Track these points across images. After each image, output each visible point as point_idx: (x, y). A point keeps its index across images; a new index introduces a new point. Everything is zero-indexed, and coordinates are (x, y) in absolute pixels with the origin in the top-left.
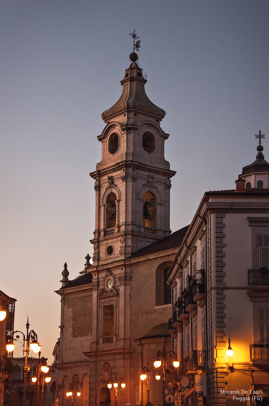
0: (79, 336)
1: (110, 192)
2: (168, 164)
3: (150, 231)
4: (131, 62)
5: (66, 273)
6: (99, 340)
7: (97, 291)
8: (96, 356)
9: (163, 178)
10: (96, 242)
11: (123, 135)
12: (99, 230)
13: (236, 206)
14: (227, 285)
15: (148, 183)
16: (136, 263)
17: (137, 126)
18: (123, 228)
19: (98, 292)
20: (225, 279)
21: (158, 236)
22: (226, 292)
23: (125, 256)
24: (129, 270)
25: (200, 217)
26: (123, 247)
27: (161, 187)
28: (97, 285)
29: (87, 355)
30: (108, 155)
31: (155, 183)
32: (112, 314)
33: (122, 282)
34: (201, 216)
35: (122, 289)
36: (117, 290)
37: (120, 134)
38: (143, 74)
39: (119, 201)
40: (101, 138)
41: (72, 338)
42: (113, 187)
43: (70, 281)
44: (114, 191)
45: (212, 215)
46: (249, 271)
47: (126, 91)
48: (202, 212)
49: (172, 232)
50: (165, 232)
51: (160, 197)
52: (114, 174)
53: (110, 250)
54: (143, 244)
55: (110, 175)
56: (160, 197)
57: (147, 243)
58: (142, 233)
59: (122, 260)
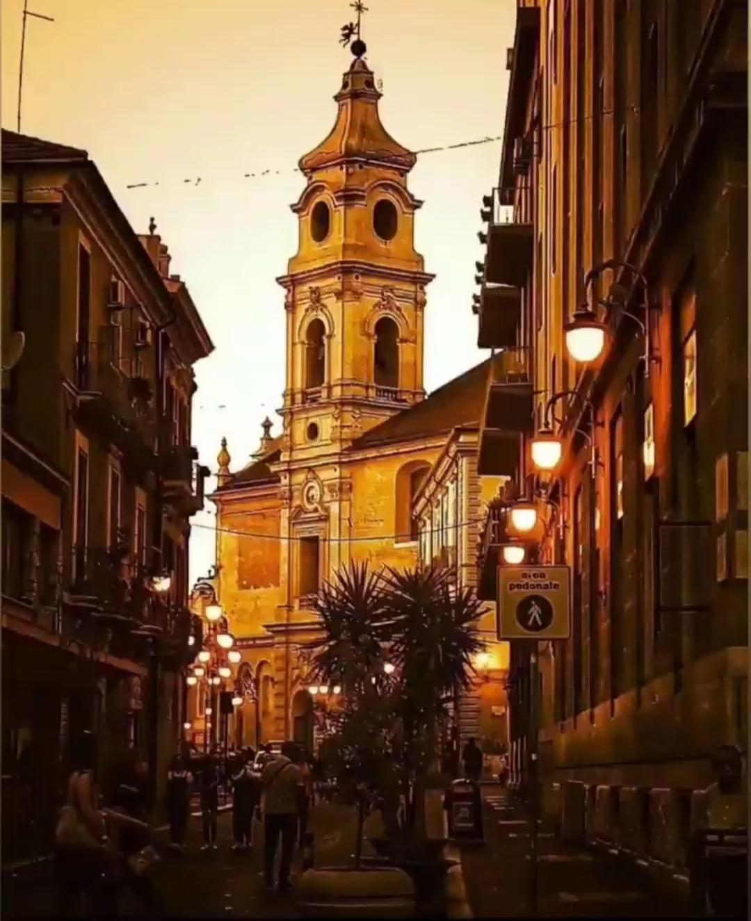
0: (252, 587)
2: (420, 260)
3: (390, 395)
6: (293, 603)
7: (287, 510)
8: (287, 632)
9: (412, 288)
10: (288, 414)
11: (337, 209)
12: (292, 389)
15: (384, 300)
17: (363, 191)
18: (337, 392)
19: (290, 511)
23: (341, 446)
24: (346, 473)
26: (336, 427)
27: (406, 306)
29: (271, 629)
33: (334, 494)
35: (334, 508)
36: (327, 509)
37: (333, 206)
39: (330, 337)
40: (296, 209)
42: (319, 308)
43: (233, 475)
45: (465, 459)
47: (343, 116)
50: (414, 394)
53: (313, 431)
55: (314, 285)
57: (382, 417)
58: (371, 399)
59: (335, 454)
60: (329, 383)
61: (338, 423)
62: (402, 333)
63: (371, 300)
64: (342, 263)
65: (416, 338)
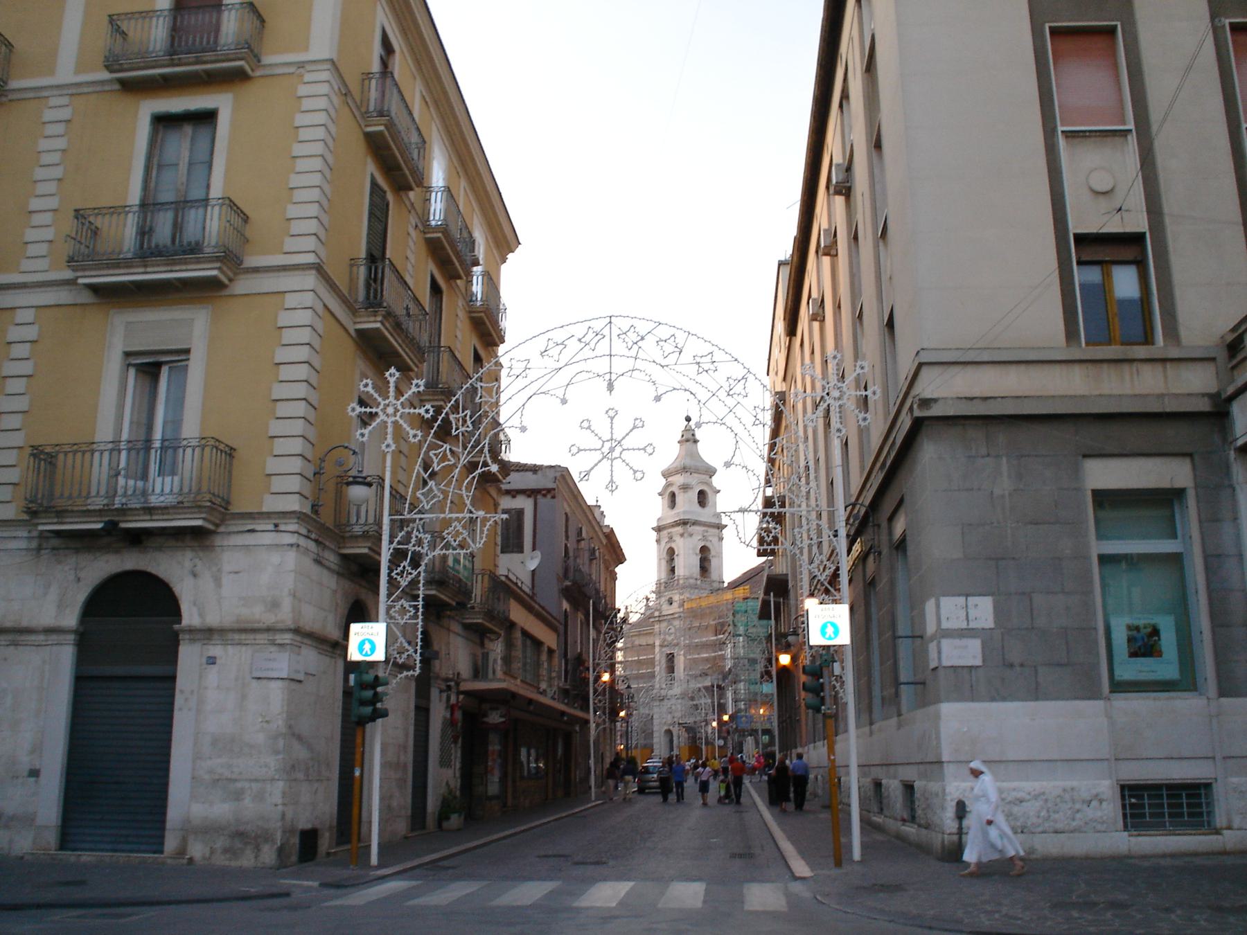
27: (715, 540)
44: (673, 545)
63: (697, 538)
65: (719, 555)
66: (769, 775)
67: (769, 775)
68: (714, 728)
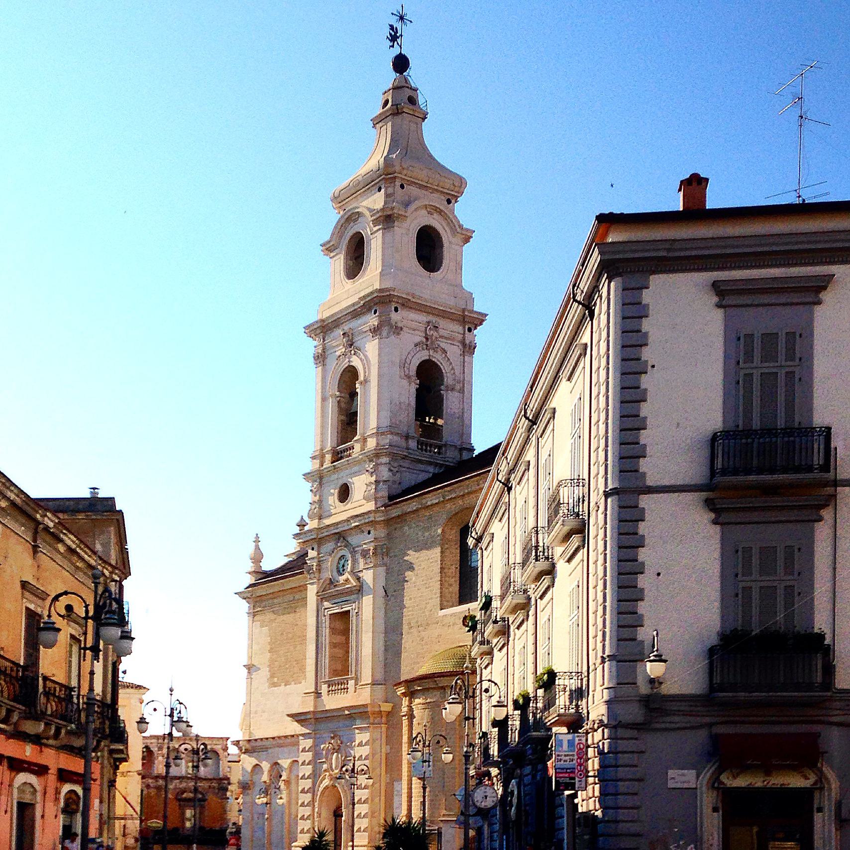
1: (346, 365)
2: (469, 297)
4: (393, 75)
5: (257, 557)
10: (318, 478)
11: (374, 236)
13: (681, 250)
14: (650, 481)
15: (427, 339)
16: (399, 516)
20: (644, 465)
21: (446, 459)
22: (646, 501)
23: (376, 504)
25: (577, 301)
27: (454, 351)
28: (316, 569)
30: (343, 282)
31: (442, 340)
32: (346, 632)
34: (578, 298)
38: (421, 100)
41: (269, 688)
44: (356, 362)
46: (714, 438)
48: (585, 285)
49: (474, 450)
50: (461, 450)
51: (452, 372)
52: (355, 324)
53: (344, 493)
54: (411, 478)
56: (452, 372)
57: (424, 474)
60: (363, 435)
61: (373, 479)
62: (448, 380)
63: (411, 338)
64: (381, 290)
65: (464, 388)
66: (436, 419)
67: (436, 419)
68: (518, 773)
